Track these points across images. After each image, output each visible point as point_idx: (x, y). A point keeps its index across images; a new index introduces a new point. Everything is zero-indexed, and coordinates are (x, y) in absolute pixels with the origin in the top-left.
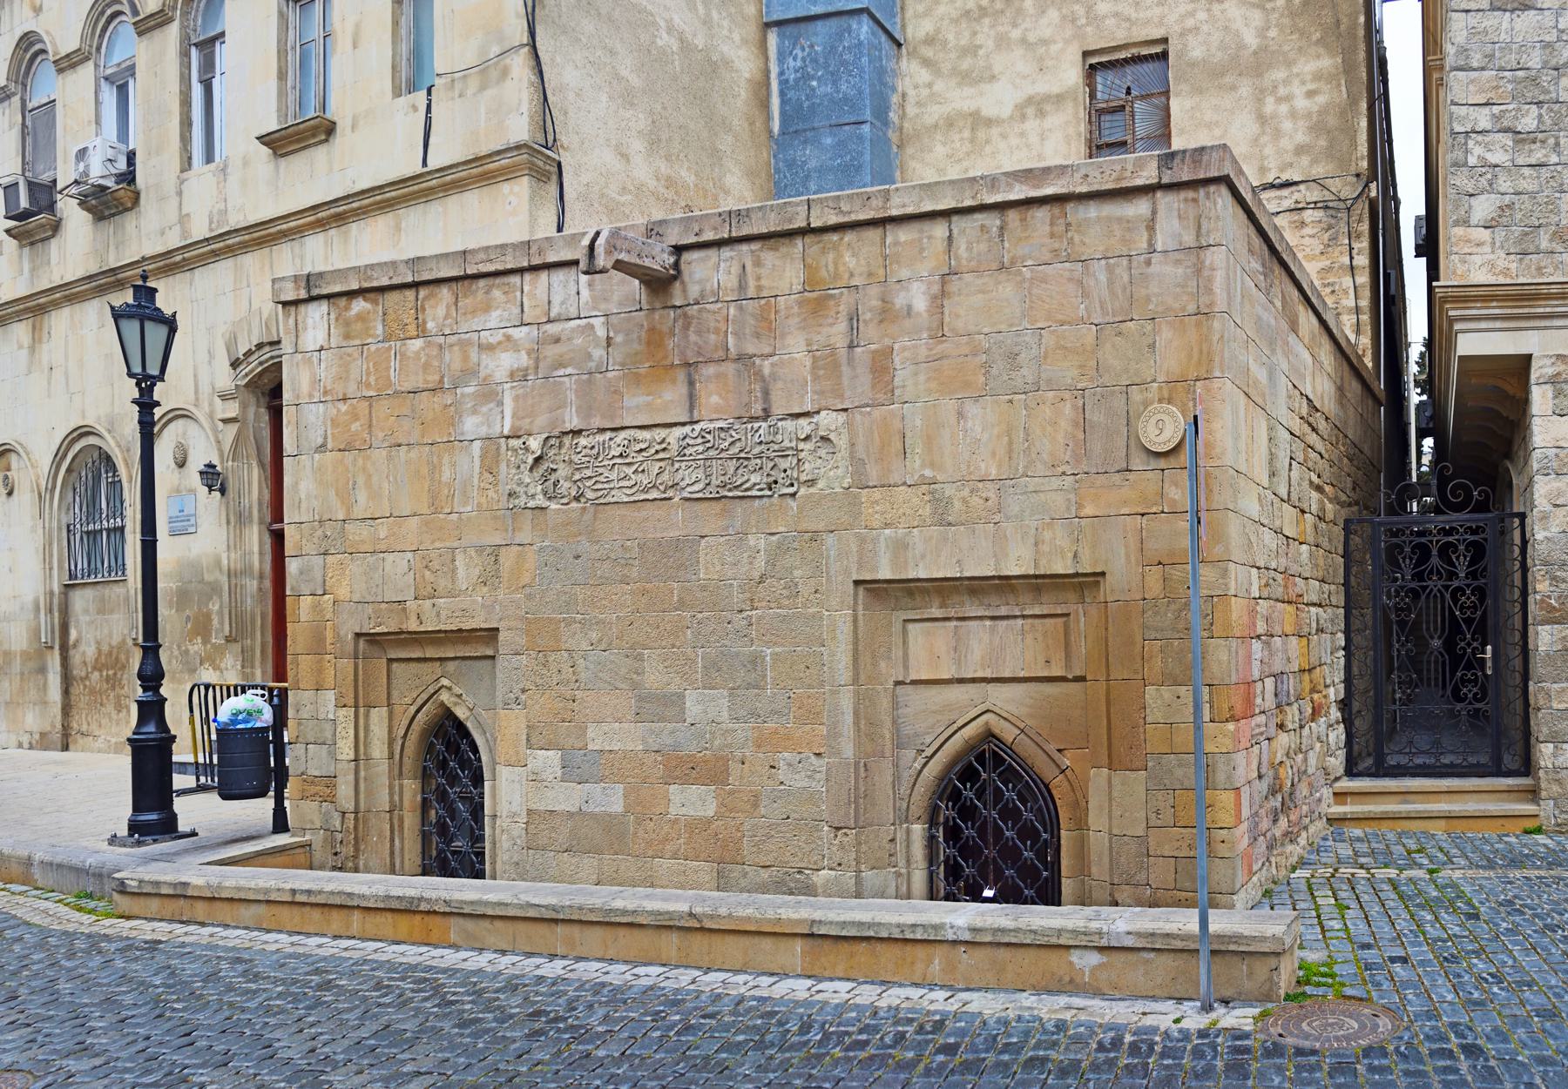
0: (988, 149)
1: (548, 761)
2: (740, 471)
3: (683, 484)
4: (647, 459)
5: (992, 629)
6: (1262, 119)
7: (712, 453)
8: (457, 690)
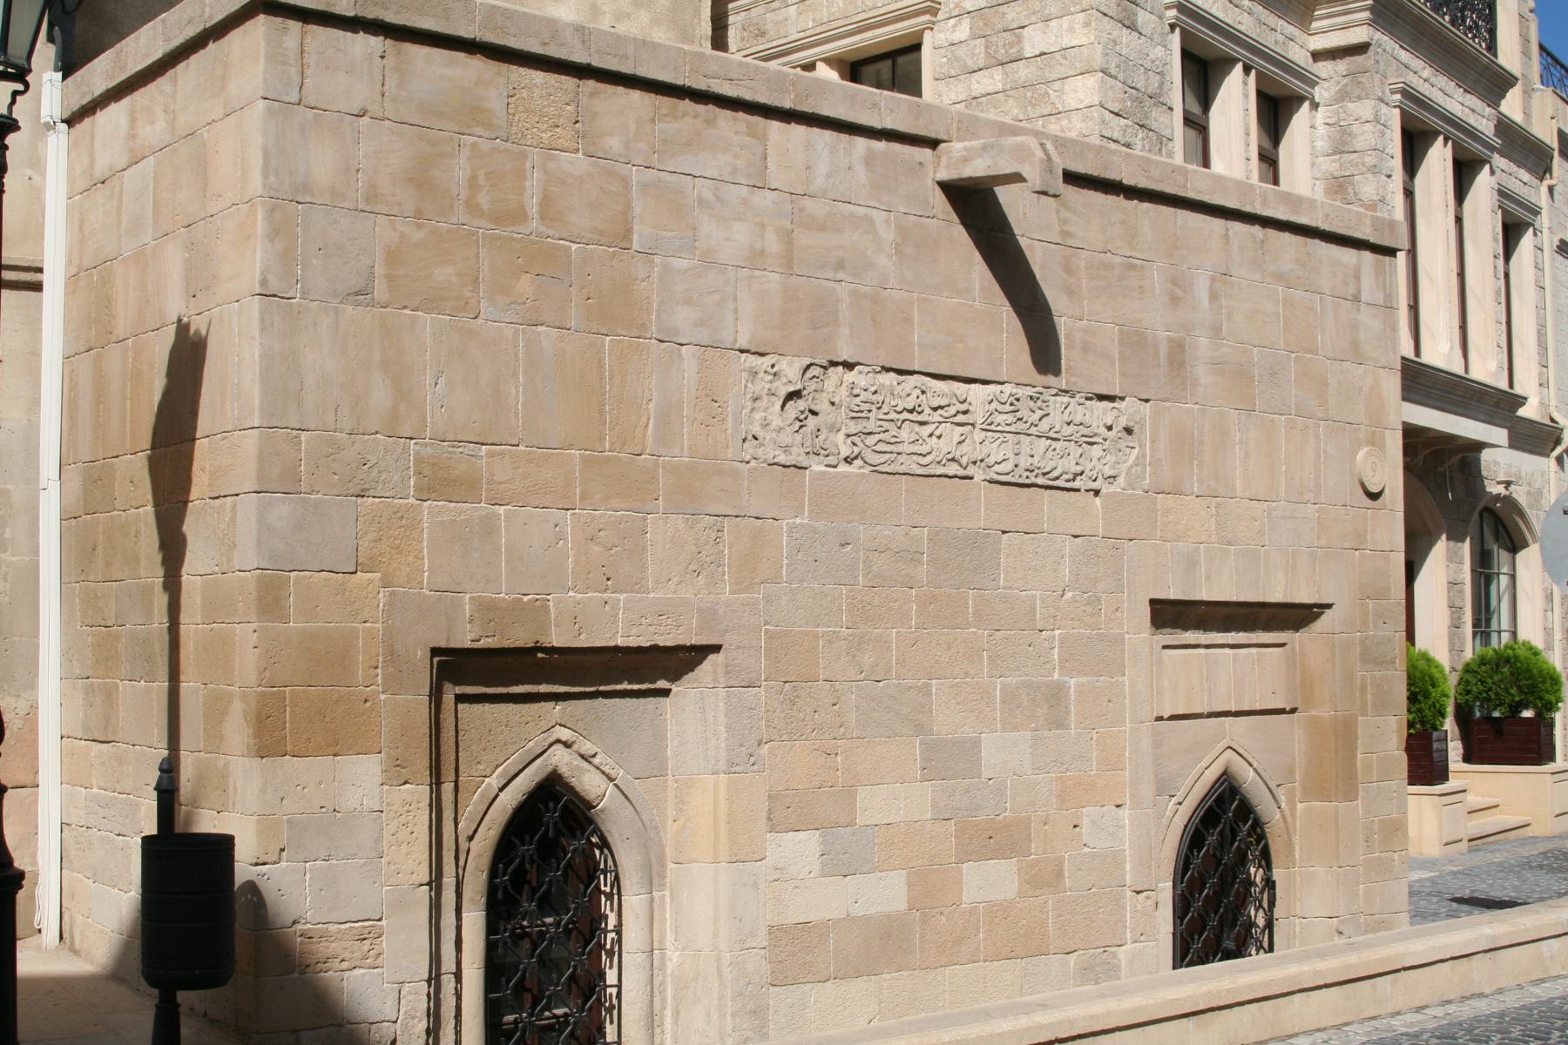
2: (1050, 454)
3: (991, 460)
4: (946, 420)
7: (1020, 426)
8: (587, 747)
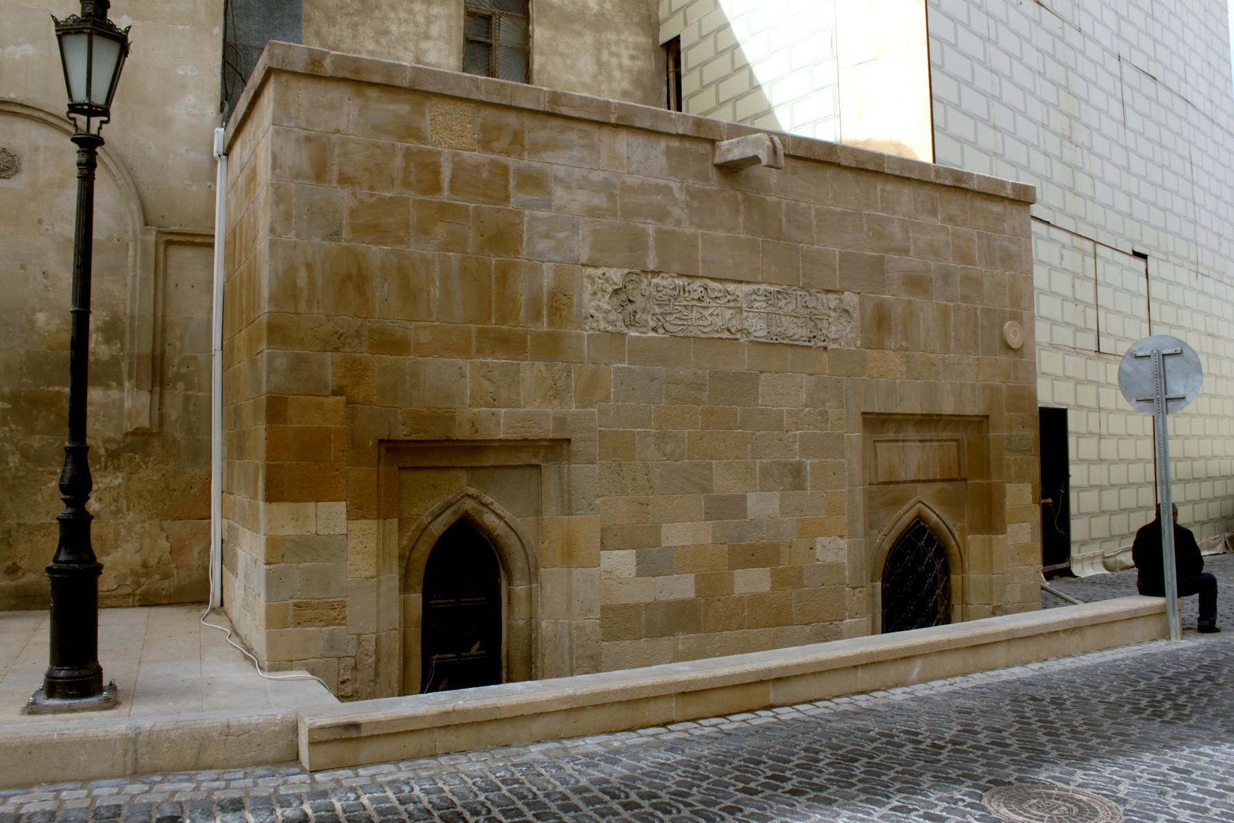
0: (377, 14)
1: (621, 561)
5: (923, 448)
6: (599, 63)
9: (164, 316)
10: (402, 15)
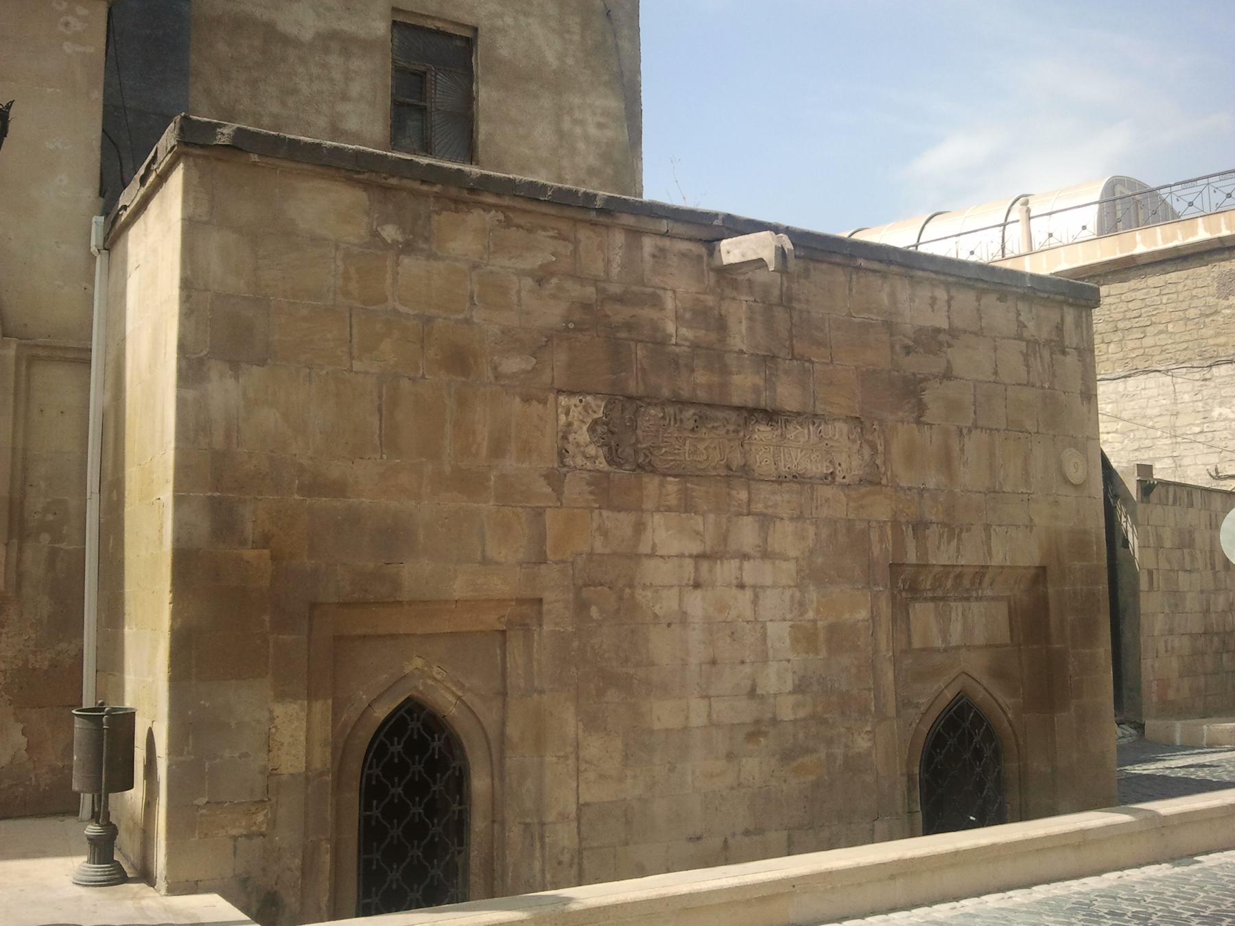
6: (561, 134)
9: (25, 450)
10: (315, 70)
